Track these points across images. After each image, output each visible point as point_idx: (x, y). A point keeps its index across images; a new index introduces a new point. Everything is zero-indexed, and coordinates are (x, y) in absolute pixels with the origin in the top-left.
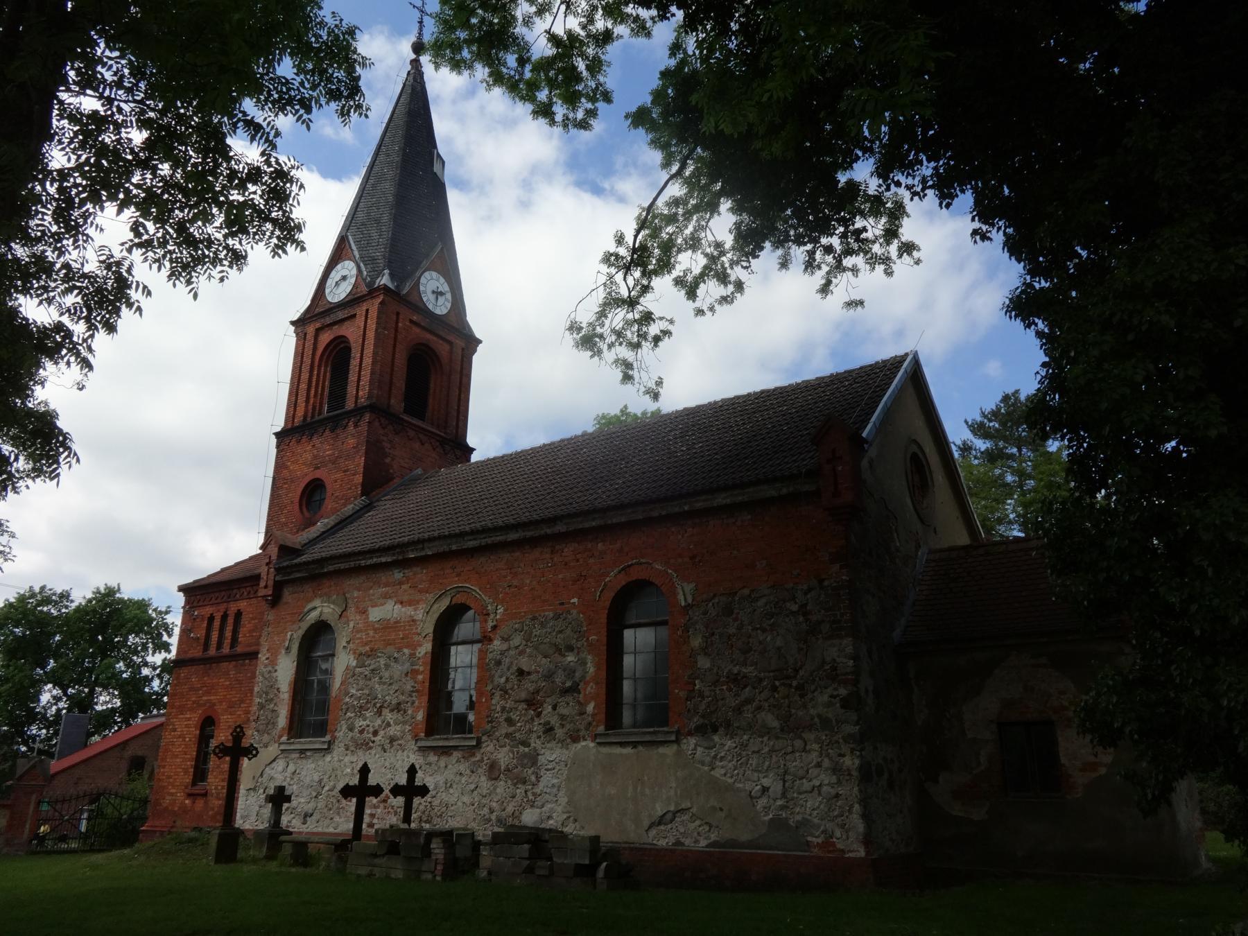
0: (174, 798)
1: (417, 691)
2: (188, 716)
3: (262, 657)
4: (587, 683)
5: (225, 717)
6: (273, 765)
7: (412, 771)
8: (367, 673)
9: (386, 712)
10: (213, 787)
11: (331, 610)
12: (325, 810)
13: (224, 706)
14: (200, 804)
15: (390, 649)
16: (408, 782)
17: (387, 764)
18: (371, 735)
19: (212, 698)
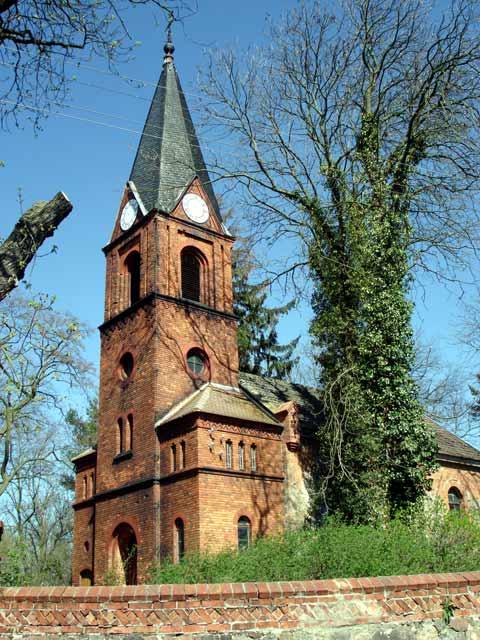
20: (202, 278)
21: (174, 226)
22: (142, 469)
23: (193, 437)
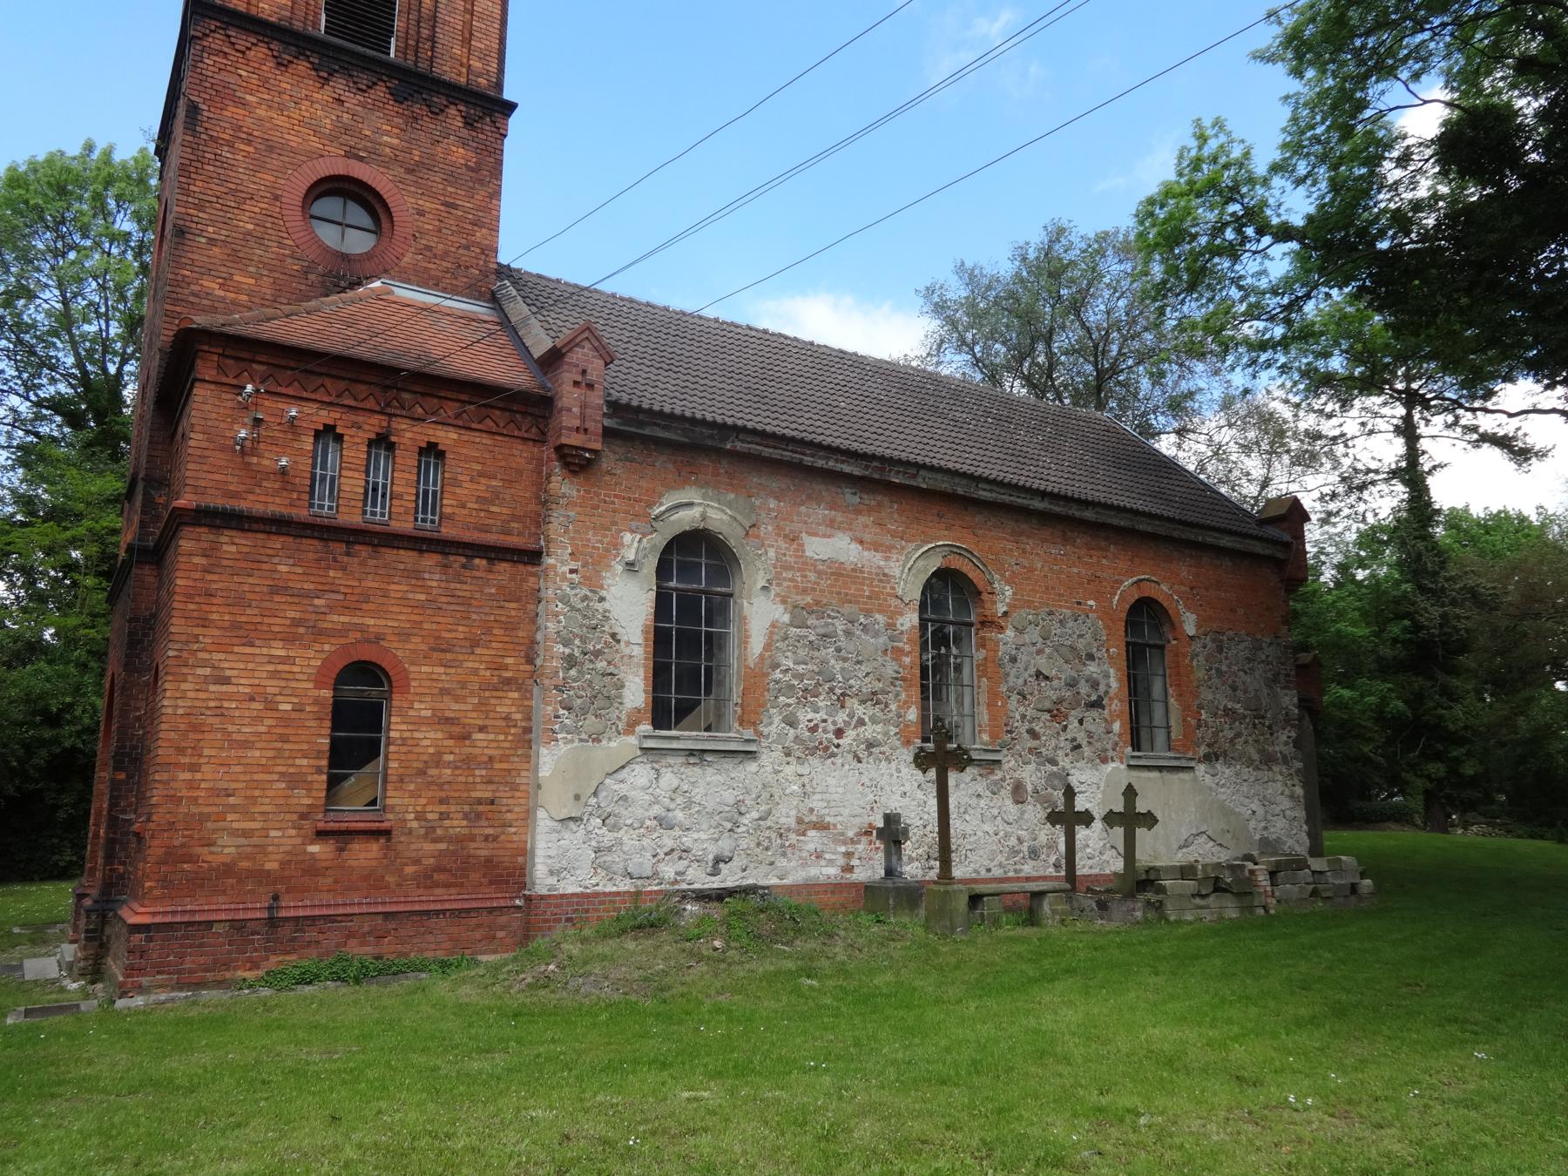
0: (255, 840)
1: (904, 679)
2: (282, 653)
3: (559, 562)
4: (1111, 699)
5: (424, 669)
6: (623, 774)
8: (812, 638)
10: (412, 816)
11: (725, 517)
14: (365, 854)
15: (847, 609)
17: (865, 779)
18: (831, 736)
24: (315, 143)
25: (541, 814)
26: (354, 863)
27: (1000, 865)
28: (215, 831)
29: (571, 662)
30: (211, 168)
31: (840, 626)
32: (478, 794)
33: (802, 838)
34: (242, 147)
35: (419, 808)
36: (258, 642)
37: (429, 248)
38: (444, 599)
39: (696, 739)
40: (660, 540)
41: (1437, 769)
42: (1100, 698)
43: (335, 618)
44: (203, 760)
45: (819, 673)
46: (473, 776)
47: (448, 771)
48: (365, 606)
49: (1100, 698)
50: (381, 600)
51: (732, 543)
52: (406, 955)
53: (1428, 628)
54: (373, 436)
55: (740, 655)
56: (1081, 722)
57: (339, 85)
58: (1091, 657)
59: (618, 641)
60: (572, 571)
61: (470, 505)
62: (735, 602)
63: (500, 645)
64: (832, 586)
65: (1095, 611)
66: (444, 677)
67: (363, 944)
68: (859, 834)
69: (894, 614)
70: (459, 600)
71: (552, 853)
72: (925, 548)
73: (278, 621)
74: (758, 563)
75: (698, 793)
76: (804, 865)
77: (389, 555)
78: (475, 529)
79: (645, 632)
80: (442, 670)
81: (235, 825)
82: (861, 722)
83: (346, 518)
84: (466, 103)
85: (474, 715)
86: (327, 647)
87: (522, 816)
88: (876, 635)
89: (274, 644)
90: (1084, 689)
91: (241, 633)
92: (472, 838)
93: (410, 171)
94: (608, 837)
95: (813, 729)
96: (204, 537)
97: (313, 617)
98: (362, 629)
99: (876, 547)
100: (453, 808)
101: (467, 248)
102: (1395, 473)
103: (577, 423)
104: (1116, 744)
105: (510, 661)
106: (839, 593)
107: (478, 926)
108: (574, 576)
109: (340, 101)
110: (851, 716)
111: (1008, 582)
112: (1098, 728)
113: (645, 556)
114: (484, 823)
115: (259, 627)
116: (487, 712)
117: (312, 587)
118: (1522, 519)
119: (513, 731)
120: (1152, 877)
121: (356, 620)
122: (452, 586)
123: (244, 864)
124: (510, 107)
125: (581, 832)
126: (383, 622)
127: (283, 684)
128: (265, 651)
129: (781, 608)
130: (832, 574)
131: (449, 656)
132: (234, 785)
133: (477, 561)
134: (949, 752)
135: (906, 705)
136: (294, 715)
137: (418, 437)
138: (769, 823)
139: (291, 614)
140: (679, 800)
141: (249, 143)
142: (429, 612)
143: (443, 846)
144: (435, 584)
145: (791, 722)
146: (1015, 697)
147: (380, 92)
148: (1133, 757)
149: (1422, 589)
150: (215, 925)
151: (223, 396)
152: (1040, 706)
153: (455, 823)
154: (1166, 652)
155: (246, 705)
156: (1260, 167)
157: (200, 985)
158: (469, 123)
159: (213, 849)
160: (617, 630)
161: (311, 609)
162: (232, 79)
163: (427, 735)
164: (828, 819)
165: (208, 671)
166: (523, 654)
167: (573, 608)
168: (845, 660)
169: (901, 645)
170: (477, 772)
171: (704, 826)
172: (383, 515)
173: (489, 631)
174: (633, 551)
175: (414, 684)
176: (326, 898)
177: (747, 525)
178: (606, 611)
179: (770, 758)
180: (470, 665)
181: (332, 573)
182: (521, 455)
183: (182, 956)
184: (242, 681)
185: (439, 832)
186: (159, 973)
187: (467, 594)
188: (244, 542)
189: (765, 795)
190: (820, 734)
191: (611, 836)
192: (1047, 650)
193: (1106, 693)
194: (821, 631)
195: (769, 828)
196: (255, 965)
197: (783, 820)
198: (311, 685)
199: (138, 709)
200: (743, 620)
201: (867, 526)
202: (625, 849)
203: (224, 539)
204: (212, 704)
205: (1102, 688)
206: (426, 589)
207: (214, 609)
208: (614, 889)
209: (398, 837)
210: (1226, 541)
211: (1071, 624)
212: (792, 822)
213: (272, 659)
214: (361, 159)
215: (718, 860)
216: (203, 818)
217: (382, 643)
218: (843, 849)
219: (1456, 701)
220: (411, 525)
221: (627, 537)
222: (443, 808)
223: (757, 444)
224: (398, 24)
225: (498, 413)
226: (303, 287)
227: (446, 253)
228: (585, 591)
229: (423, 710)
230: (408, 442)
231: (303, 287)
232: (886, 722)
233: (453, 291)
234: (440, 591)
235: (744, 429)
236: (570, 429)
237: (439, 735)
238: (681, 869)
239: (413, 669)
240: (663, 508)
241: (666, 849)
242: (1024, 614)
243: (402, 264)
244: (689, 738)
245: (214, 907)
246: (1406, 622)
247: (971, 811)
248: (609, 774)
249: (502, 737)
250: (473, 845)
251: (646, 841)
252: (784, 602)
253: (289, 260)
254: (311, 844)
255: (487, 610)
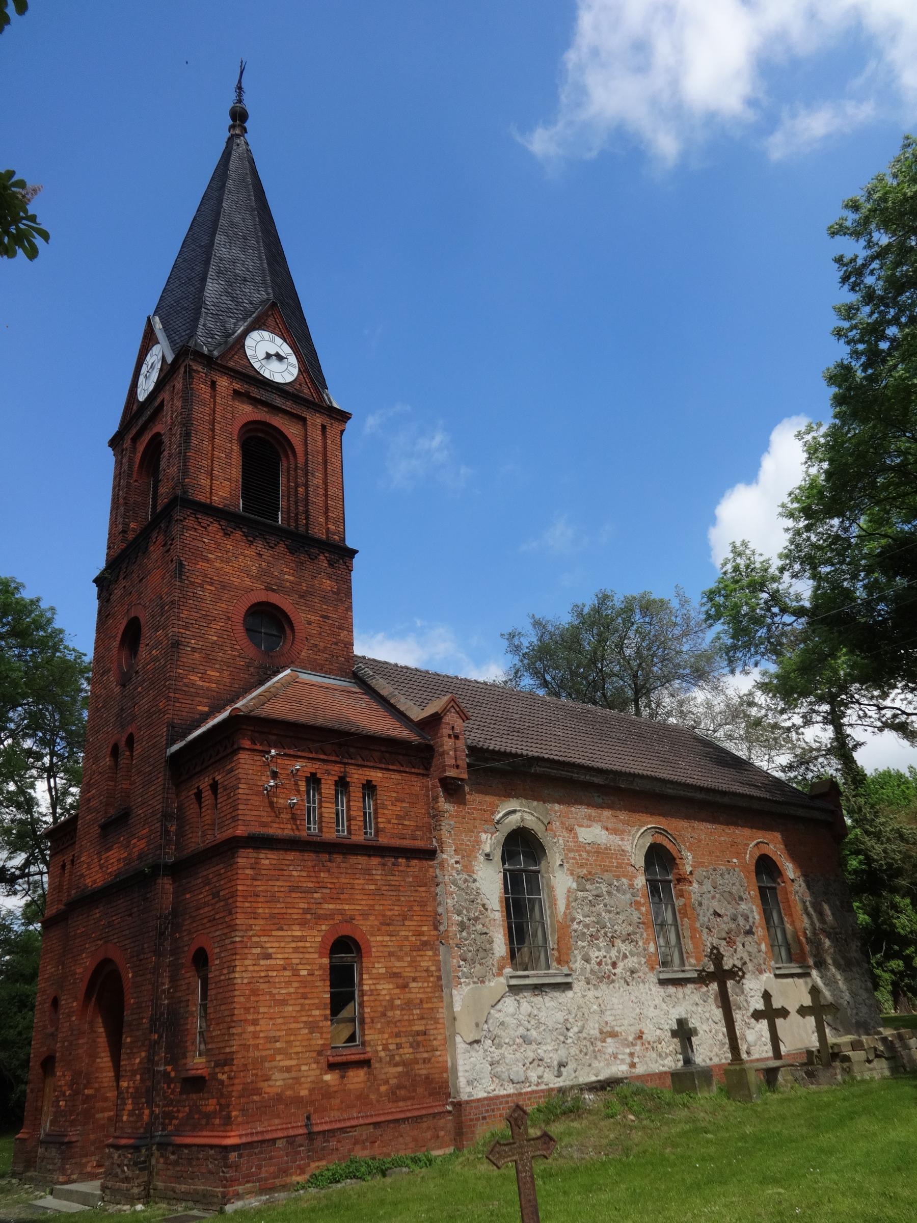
0: (293, 1074)
1: (643, 923)
2: (299, 934)
3: (449, 856)
4: (757, 927)
5: (379, 938)
6: (499, 1006)
7: (767, 996)
8: (590, 898)
9: (618, 942)
10: (380, 1048)
11: (534, 818)
12: (581, 1056)
13: (373, 921)
14: (357, 1077)
15: (606, 876)
16: (765, 1005)
17: (633, 998)
18: (610, 967)
19: (347, 907)
20: (282, 480)
21: (223, 383)
22: (142, 844)
23: (232, 770)
24: (248, 582)
25: (458, 1039)
26: (351, 1087)
27: (717, 1055)
28: (271, 1069)
29: (462, 926)
30: (191, 602)
31: (604, 888)
32: (416, 1028)
33: (604, 1044)
34: (208, 587)
35: (384, 1042)
36: (285, 927)
37: (315, 646)
38: (384, 888)
39: (538, 976)
40: (501, 836)
41: (896, 964)
42: (751, 927)
43: (326, 906)
44: (260, 1016)
45: (597, 923)
46: (413, 1014)
47: (398, 1012)
48: (342, 896)
49: (751, 927)
50: (350, 891)
51: (540, 835)
52: (389, 1155)
53: (877, 861)
54: (337, 778)
55: (552, 913)
56: (743, 945)
57: (259, 545)
58: (741, 899)
59: (487, 910)
60: (457, 862)
61: (393, 821)
62: (542, 877)
63: (418, 918)
64: (595, 861)
65: (738, 867)
66: (390, 944)
67: (364, 1148)
68: (635, 1039)
69: (632, 878)
70: (393, 888)
71: (467, 1068)
72: (642, 831)
73: (295, 911)
74: (555, 848)
75: (542, 1015)
76: (608, 1065)
77: (353, 860)
78: (397, 837)
79: (501, 902)
80: (387, 938)
81: (281, 1064)
82: (625, 956)
83: (327, 835)
84: (330, 552)
85: (408, 969)
86: (324, 927)
87: (443, 1042)
88: (624, 893)
89: (294, 927)
90: (741, 921)
91: (276, 921)
92: (415, 1061)
93: (301, 597)
94: (496, 1054)
95: (599, 964)
96: (251, 855)
97: (314, 906)
98: (342, 912)
99: (615, 831)
100: (404, 1040)
101: (336, 644)
102: (829, 751)
103: (453, 762)
104: (765, 959)
105: (425, 928)
106: (600, 865)
107: (429, 1128)
108: (458, 866)
109: (260, 555)
110: (619, 952)
111: (690, 850)
112: (752, 948)
113: (495, 849)
114: (421, 1049)
115: (285, 916)
116: (416, 967)
117: (311, 885)
118: (900, 776)
119: (431, 979)
120: (836, 1051)
121: (338, 907)
122: (389, 878)
123: (289, 1093)
124: (353, 553)
125: (481, 1051)
126: (353, 907)
127: (301, 956)
128: (289, 933)
129: (570, 878)
130: (595, 852)
131: (391, 928)
132: (279, 1034)
133: (400, 860)
134: (726, 971)
135: (647, 942)
136: (309, 978)
137: (361, 777)
138: (584, 1035)
139: (302, 905)
140: (533, 1022)
141: (211, 584)
142: (377, 898)
143: (400, 1069)
144: (379, 877)
145: (587, 960)
146: (705, 931)
147: (281, 547)
148: (777, 968)
149: (867, 833)
150: (278, 1141)
151: (256, 758)
152: (720, 936)
153: (406, 1050)
154: (778, 891)
155: (281, 973)
156: (773, 571)
157: (272, 1189)
158: (331, 565)
159: (270, 1083)
160: (486, 901)
161: (313, 901)
162: (200, 545)
163: (385, 986)
164: (617, 1029)
165: (258, 950)
166: (431, 923)
167: (460, 888)
168: (610, 912)
169: (638, 899)
170: (415, 1012)
171: (549, 1041)
172: (343, 831)
173: (411, 908)
174: (488, 845)
175: (373, 950)
176: (336, 1114)
177: (546, 823)
178: (478, 889)
179: (579, 986)
180: (403, 933)
181: (322, 875)
182: (416, 785)
183: (259, 1167)
184: (279, 956)
185: (397, 1058)
186: (248, 1182)
187: (397, 883)
188: (273, 857)
189: (580, 1014)
190: (603, 966)
191: (498, 1052)
192: (717, 896)
193: (754, 923)
194: (595, 893)
195: (585, 1038)
196: (303, 1172)
197: (592, 1032)
198: (316, 956)
199: (164, 984)
200: (551, 888)
201: (608, 818)
202: (507, 1061)
203: (262, 856)
204: (263, 974)
205: (751, 920)
206: (374, 882)
207: (260, 905)
208: (505, 1092)
209: (375, 1064)
210: (801, 812)
211: (727, 876)
212: (596, 1033)
213: (295, 939)
214: (274, 591)
215: (562, 1065)
216: (263, 1059)
217: (354, 922)
218: (628, 1051)
219: (901, 912)
220: (362, 838)
221: (484, 836)
222: (398, 1040)
223: (548, 768)
224: (282, 503)
225: (401, 757)
226: (246, 676)
227: (325, 648)
228: (465, 876)
229: (380, 968)
230: (356, 781)
231: (246, 676)
232: (638, 955)
233: (328, 673)
234: (383, 883)
235: (543, 759)
236: (450, 766)
237: (391, 986)
238: (540, 1074)
239: (372, 939)
240: (500, 815)
241: (530, 1060)
242: (700, 872)
243: (301, 657)
244: (534, 976)
245: (274, 1128)
246: (861, 857)
247: (694, 1016)
248: (493, 1006)
249: (426, 985)
250: (417, 1067)
251: (518, 1055)
252: (572, 874)
253: (238, 659)
254: (325, 1074)
255: (409, 893)
